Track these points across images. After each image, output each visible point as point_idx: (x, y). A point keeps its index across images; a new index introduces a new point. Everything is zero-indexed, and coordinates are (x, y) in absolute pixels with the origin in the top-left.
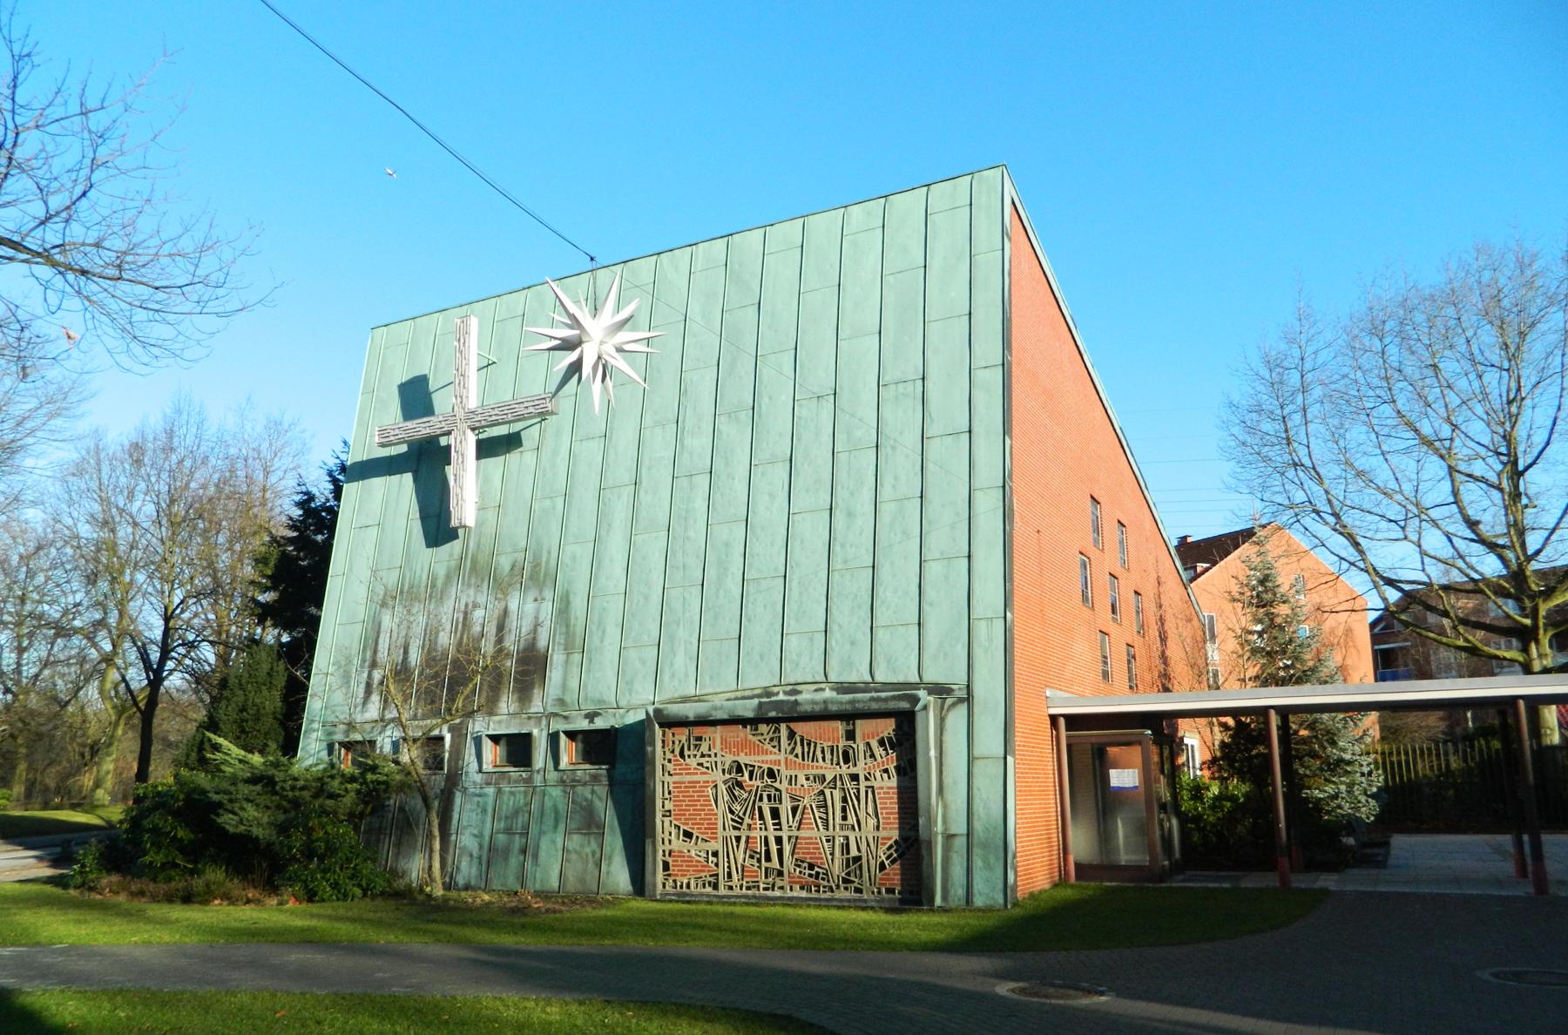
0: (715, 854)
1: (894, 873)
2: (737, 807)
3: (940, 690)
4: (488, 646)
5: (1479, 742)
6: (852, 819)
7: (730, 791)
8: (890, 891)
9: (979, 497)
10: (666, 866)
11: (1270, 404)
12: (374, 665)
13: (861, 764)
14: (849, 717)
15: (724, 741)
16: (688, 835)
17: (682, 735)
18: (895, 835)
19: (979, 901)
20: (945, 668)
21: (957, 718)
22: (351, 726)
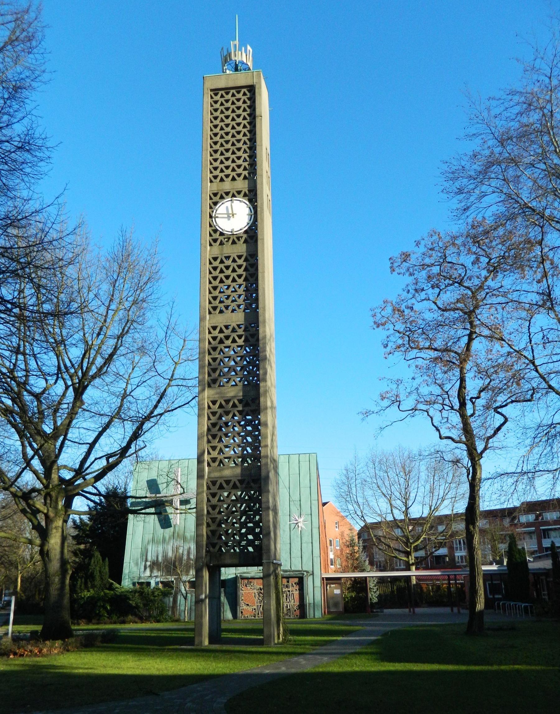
0: (255, 609)
1: (298, 612)
2: (260, 598)
3: (307, 572)
4: (185, 557)
5: (190, 618)
6: (288, 600)
7: (259, 594)
8: (297, 616)
9: (314, 530)
10: (242, 612)
11: (345, 480)
12: (146, 561)
13: (290, 588)
14: (288, 578)
15: (257, 583)
16: (248, 605)
17: (246, 581)
18: (298, 604)
19: (316, 617)
20: (307, 567)
21: (310, 578)
22: (140, 578)
